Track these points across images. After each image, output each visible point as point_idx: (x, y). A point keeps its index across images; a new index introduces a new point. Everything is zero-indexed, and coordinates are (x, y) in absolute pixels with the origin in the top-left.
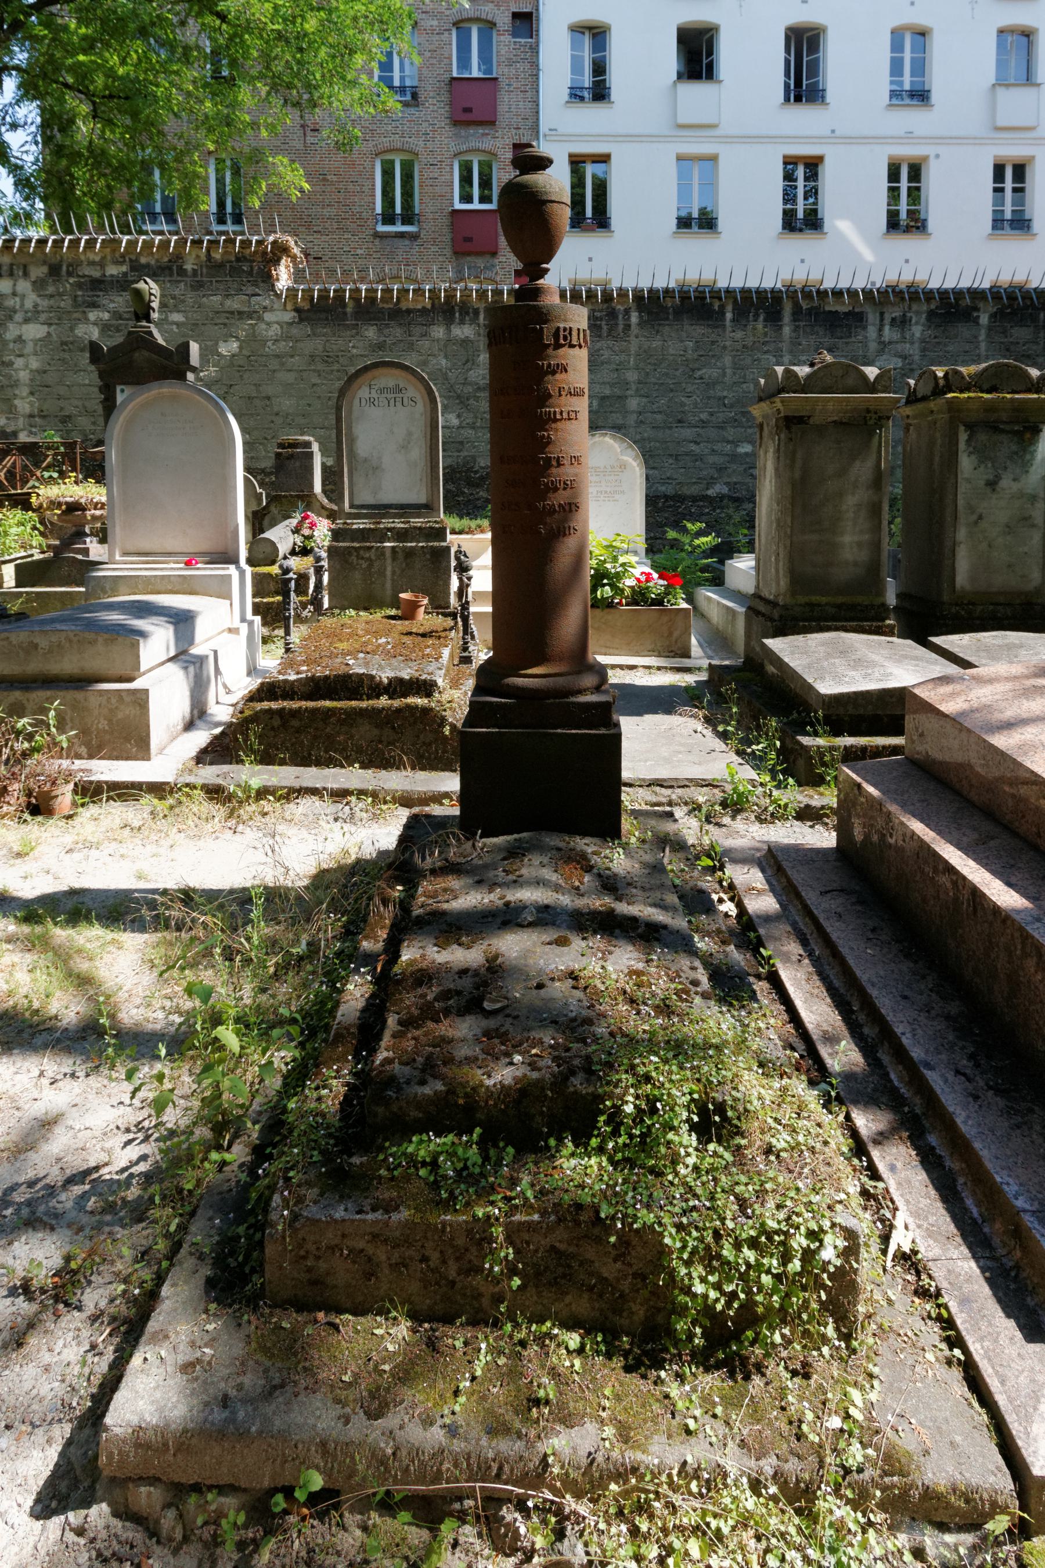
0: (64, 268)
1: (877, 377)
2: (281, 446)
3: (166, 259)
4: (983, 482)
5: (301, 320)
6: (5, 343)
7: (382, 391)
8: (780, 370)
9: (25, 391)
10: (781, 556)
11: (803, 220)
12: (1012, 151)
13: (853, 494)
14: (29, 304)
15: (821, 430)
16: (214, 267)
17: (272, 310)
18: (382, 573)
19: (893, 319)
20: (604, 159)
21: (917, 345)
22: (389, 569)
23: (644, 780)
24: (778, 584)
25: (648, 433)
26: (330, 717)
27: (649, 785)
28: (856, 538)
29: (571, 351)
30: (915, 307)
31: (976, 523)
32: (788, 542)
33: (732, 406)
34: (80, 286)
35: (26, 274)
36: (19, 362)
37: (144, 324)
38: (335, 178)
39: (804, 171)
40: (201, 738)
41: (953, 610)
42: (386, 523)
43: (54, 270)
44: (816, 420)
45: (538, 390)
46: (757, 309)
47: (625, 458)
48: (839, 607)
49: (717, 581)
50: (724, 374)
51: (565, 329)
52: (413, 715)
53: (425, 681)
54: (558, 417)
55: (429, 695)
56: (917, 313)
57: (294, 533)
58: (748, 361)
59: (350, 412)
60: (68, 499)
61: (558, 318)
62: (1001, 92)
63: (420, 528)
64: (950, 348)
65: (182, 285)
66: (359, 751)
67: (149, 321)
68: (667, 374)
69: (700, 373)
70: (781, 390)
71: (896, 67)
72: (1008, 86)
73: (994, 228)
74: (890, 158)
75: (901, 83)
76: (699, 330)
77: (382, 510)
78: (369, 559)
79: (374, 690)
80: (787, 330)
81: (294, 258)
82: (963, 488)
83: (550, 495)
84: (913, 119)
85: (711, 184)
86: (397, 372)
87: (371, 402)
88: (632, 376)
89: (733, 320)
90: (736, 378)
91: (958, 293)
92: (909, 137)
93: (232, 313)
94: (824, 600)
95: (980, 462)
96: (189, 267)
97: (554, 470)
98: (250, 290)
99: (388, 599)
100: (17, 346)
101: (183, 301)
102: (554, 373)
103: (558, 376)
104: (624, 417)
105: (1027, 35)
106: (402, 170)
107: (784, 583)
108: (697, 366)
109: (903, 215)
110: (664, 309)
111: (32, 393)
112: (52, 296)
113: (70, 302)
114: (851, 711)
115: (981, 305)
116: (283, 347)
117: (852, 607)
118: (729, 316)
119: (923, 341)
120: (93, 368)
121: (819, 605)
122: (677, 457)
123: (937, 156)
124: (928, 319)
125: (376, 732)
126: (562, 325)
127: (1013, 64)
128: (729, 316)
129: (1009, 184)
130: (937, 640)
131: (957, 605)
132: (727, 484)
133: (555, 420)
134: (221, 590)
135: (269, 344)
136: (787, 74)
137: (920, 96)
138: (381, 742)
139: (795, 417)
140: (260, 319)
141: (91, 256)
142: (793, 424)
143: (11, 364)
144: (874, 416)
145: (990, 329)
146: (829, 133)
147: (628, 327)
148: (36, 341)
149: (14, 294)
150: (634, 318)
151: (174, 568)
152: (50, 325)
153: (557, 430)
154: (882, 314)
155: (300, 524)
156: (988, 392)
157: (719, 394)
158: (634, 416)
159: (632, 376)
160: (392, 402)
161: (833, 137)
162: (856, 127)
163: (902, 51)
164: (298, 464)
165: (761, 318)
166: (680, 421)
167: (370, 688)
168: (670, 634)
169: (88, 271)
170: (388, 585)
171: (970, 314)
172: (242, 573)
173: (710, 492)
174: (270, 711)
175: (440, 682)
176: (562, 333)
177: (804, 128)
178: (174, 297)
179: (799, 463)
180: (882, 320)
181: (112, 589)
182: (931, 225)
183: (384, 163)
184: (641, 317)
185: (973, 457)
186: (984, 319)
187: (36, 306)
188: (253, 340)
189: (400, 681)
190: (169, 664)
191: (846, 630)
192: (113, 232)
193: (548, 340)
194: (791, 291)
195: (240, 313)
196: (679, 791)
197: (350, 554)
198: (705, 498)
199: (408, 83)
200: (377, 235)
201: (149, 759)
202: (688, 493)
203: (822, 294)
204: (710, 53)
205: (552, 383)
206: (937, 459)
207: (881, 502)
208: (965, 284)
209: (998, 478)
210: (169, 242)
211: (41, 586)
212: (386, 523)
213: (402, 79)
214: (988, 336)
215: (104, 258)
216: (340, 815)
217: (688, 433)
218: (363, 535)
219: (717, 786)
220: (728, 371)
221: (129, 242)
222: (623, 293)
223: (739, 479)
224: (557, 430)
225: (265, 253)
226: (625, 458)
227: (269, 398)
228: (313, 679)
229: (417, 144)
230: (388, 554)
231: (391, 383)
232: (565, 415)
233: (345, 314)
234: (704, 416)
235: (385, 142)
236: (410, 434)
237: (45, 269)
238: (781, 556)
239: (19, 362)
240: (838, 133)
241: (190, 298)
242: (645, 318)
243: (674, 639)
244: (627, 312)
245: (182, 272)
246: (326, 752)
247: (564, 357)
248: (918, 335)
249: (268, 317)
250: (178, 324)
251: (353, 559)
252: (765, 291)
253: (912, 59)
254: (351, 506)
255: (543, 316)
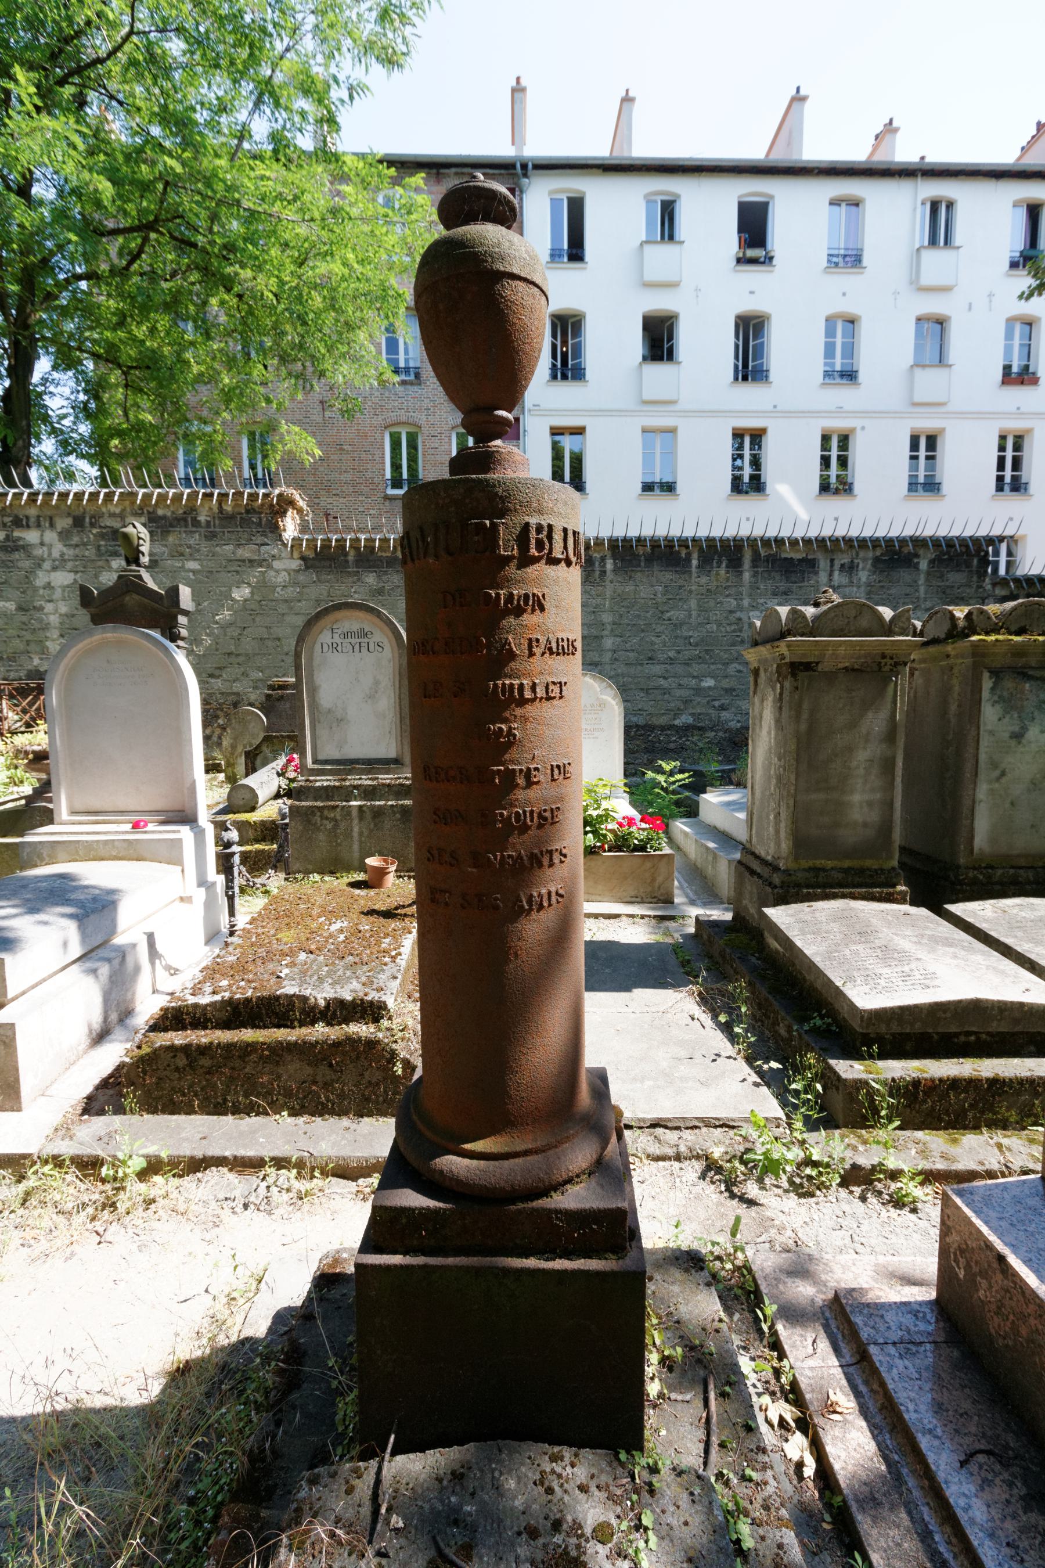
0: (87, 520)
1: (893, 618)
2: (271, 687)
3: (181, 511)
4: (1007, 735)
5: (307, 568)
6: (35, 589)
7: (345, 635)
8: (784, 611)
9: (55, 634)
10: (783, 816)
11: (749, 483)
12: (927, 423)
13: (865, 748)
14: (56, 554)
15: (831, 677)
16: (226, 519)
17: (280, 558)
18: (348, 835)
19: (842, 566)
20: (579, 431)
21: (863, 589)
22: (356, 829)
23: (643, 1120)
24: (778, 844)
25: (622, 669)
26: (249, 1054)
27: (654, 1126)
28: (866, 797)
29: (552, 571)
30: (862, 554)
31: (998, 779)
32: (791, 802)
33: (697, 645)
34: (102, 536)
35: (52, 525)
36: (49, 607)
37: (134, 567)
38: (350, 448)
39: (749, 441)
40: (114, 1054)
41: (971, 875)
42: (353, 780)
43: (78, 522)
44: (825, 667)
45: (489, 646)
46: (720, 556)
47: (604, 697)
48: (846, 871)
49: (691, 811)
50: (690, 616)
51: (539, 529)
52: (354, 1049)
53: (371, 1003)
54: (528, 694)
55: (376, 1020)
56: (865, 560)
57: (279, 775)
58: (712, 604)
59: (310, 659)
60: (36, 748)
61: (526, 506)
62: (918, 371)
63: (389, 785)
64: (893, 591)
65: (197, 536)
66: (288, 1094)
67: (139, 565)
68: (638, 616)
69: (668, 615)
70: (789, 633)
71: (829, 351)
72: (924, 366)
73: (910, 490)
74: (823, 429)
75: (833, 364)
76: (668, 576)
77: (348, 765)
78: (335, 820)
79: (308, 1015)
80: (747, 576)
81: (300, 511)
82: (985, 742)
83: (514, 839)
84: (843, 396)
85: (670, 454)
86: (361, 614)
87: (334, 647)
88: (607, 618)
89: (698, 567)
90: (700, 620)
91: (903, 541)
92: (840, 411)
93: (243, 561)
94: (829, 864)
95: (1006, 712)
96: (202, 518)
97: (520, 794)
98: (259, 539)
99: (356, 863)
100: (47, 592)
101: (198, 551)
102: (519, 612)
103: (528, 619)
104: (600, 655)
105: (941, 322)
106: (408, 441)
107: (785, 846)
108: (665, 608)
109: (833, 480)
110: (636, 557)
111: (62, 636)
112: (77, 546)
113: (94, 551)
114: (895, 1028)
115: (921, 552)
116: (291, 592)
117: (861, 871)
118: (695, 562)
119: (869, 585)
120: (84, 611)
121: (824, 870)
122: (647, 691)
123: (863, 428)
124: (874, 565)
125: (309, 1070)
126: (533, 521)
127: (928, 348)
128: (695, 562)
129: (922, 453)
130: (952, 908)
131: (974, 868)
132: (692, 715)
133: (523, 702)
134: (171, 854)
135: (278, 589)
136: (737, 357)
137: (850, 375)
138: (315, 1083)
139: (801, 663)
140: (270, 567)
141: (112, 509)
142: (799, 670)
143: (41, 609)
144: (890, 662)
145: (928, 573)
146: (771, 408)
147: (603, 573)
148: (64, 588)
149: (42, 544)
150: (609, 565)
151: (119, 830)
152: (76, 572)
153: (525, 719)
154: (832, 561)
155: (285, 768)
156: (1018, 633)
157: (686, 634)
158: (610, 654)
159: (607, 618)
160: (357, 647)
161: (775, 412)
162: (794, 400)
163: (834, 336)
164: (288, 705)
165: (724, 565)
166: (650, 659)
167: (302, 1011)
168: (653, 880)
169: (109, 522)
170: (356, 847)
171: (910, 560)
172: (199, 834)
173: (677, 722)
174: (172, 1049)
175: (391, 1003)
176: (533, 534)
177: (750, 404)
178: (189, 547)
179: (805, 716)
180: (832, 566)
181: (49, 856)
182: (857, 488)
183: (391, 435)
184: (615, 564)
185: (998, 707)
186: (924, 565)
187: (62, 555)
188: (263, 587)
189: (341, 1003)
190: (74, 967)
191: (854, 897)
192: (131, 486)
193: (508, 547)
194: (752, 541)
195: (250, 561)
196: (687, 1134)
197: (313, 814)
198: (672, 727)
199: (412, 364)
200: (387, 498)
201: (19, 1110)
202: (657, 723)
203: (779, 541)
204: (671, 338)
205: (517, 631)
206: (953, 708)
207: (894, 758)
208: (908, 532)
209: (1024, 729)
210: (182, 494)
211: (12, 836)
212: (353, 780)
213: (407, 360)
214: (927, 580)
215: (123, 510)
216: (252, 1199)
217: (657, 669)
218: (327, 793)
219: (733, 1127)
220: (694, 613)
221: (145, 495)
222: (599, 542)
223: (704, 711)
224: (525, 719)
225: (272, 505)
226: (604, 697)
227: (279, 639)
228: (230, 1002)
229: (421, 418)
230: (355, 813)
231: (355, 627)
232: (540, 692)
233: (347, 561)
234: (671, 654)
235: (393, 417)
236: (377, 683)
237: (70, 521)
238: (783, 816)
239: (49, 607)
240: (779, 408)
241: (205, 547)
242: (619, 565)
243: (657, 885)
244: (603, 559)
245: (196, 523)
246: (246, 1096)
247: (538, 581)
248: (864, 579)
249: (276, 564)
250: (194, 572)
251: (317, 819)
252: (728, 540)
253: (843, 344)
254: (315, 761)
255: (497, 502)
